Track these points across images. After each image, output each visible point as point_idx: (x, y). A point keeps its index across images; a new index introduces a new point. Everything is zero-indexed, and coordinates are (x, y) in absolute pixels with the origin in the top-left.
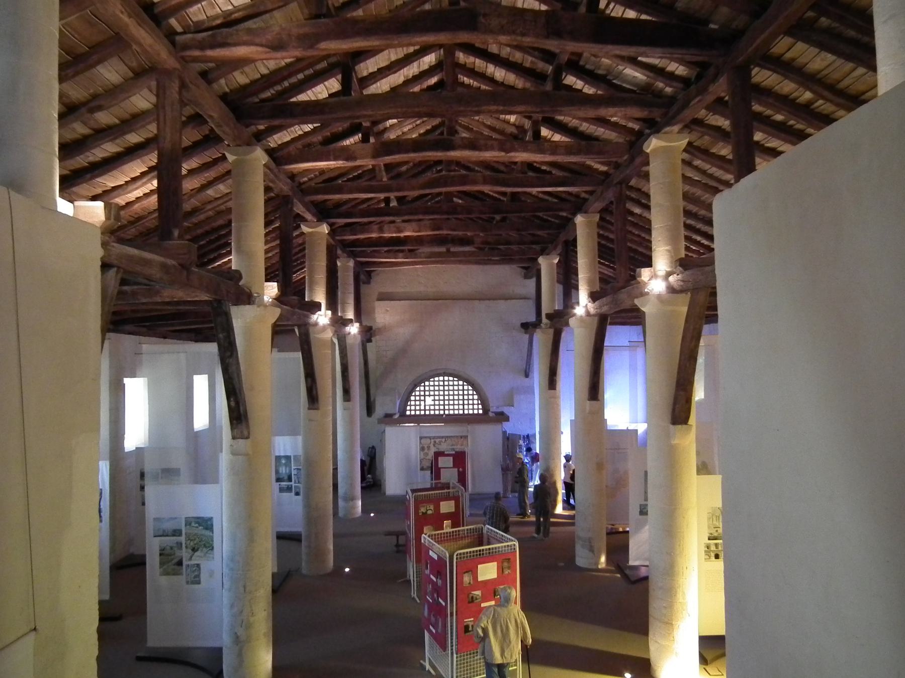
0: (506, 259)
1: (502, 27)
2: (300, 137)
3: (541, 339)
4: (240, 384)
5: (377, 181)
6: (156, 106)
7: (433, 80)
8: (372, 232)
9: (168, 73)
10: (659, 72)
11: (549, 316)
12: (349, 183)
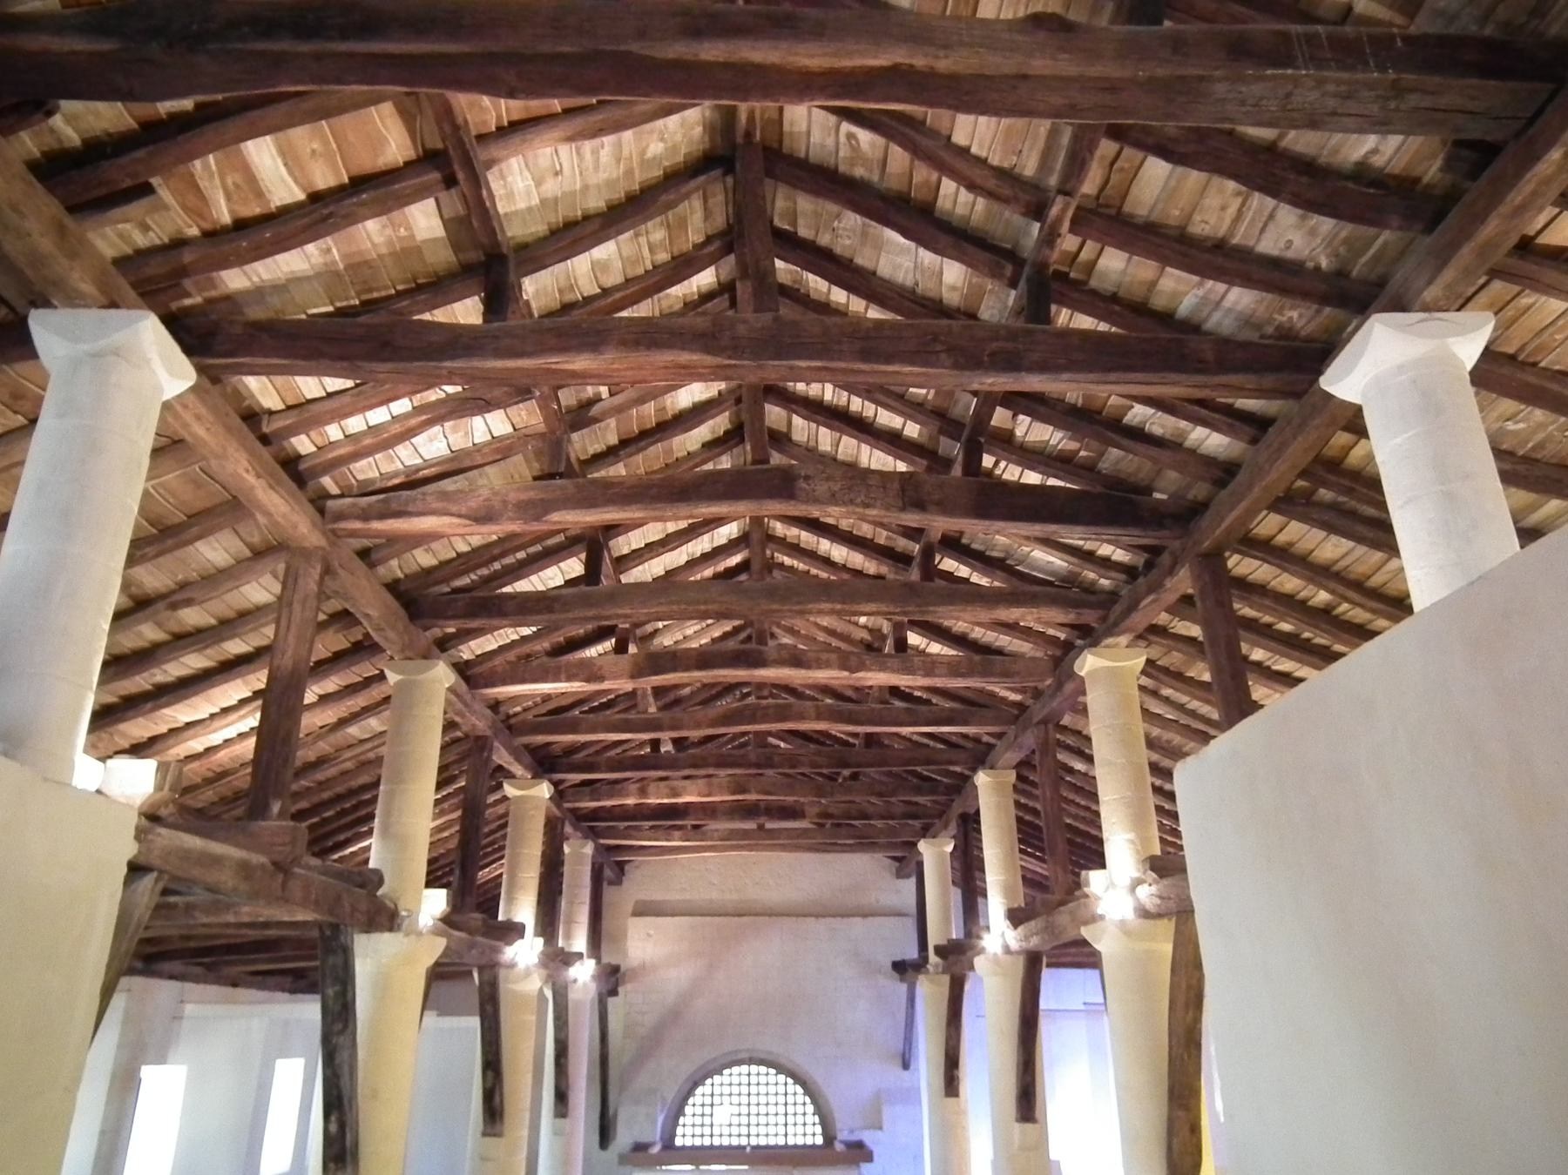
0: (865, 843)
1: (833, 495)
2: (513, 645)
3: (930, 991)
4: (352, 1085)
5: (639, 713)
6: (280, 598)
7: (735, 560)
8: (627, 795)
9: (306, 553)
10: (1088, 557)
11: (940, 951)
12: (591, 716)
